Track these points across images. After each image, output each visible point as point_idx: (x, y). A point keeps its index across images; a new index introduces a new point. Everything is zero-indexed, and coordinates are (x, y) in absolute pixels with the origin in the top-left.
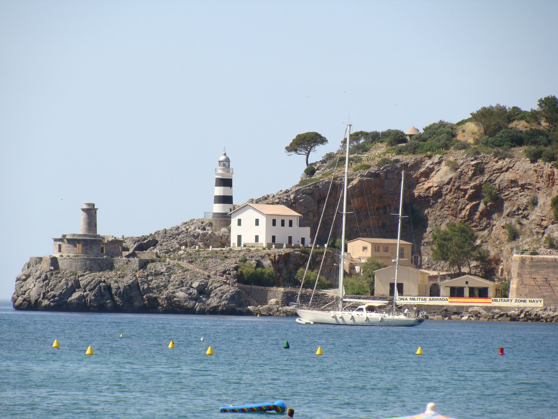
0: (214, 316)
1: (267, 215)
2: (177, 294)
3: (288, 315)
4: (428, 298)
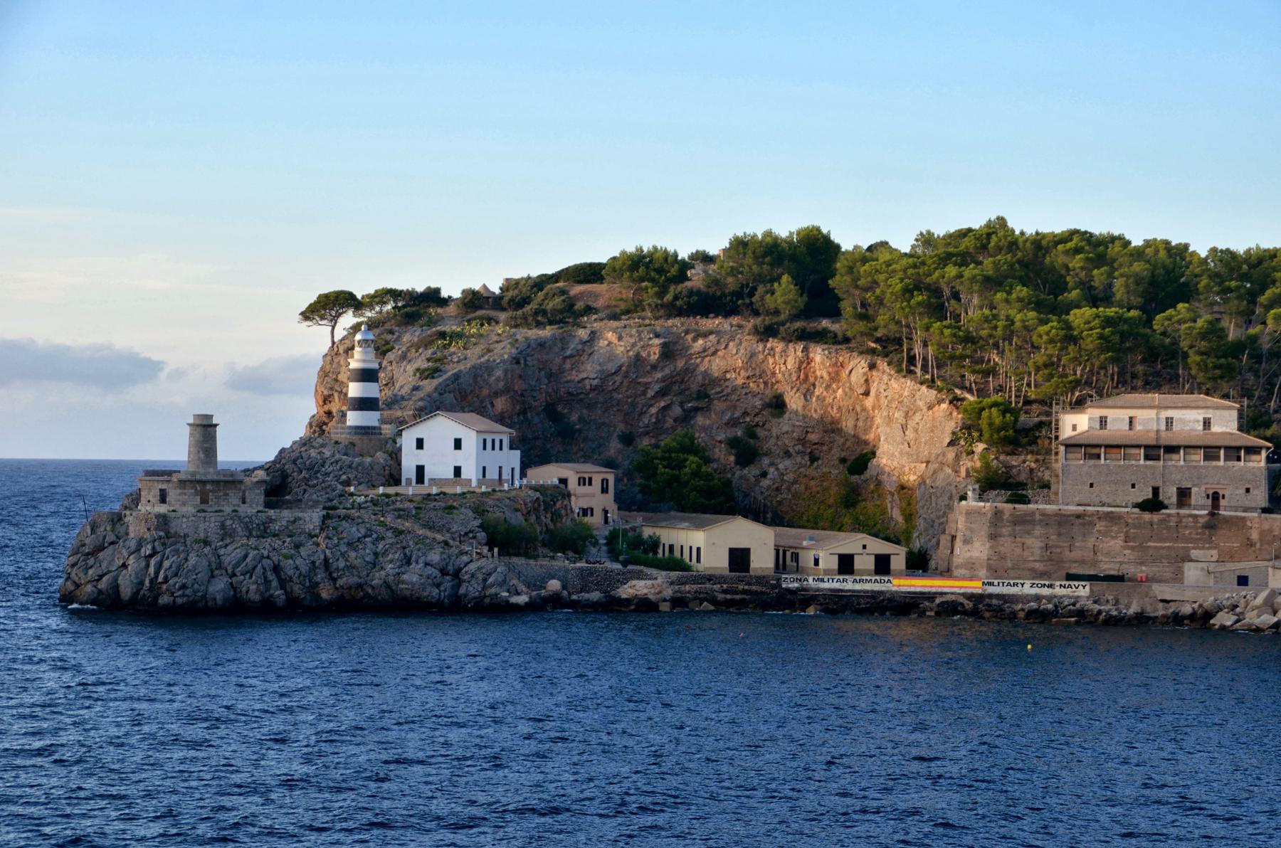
2: (405, 577)
4: (1028, 583)
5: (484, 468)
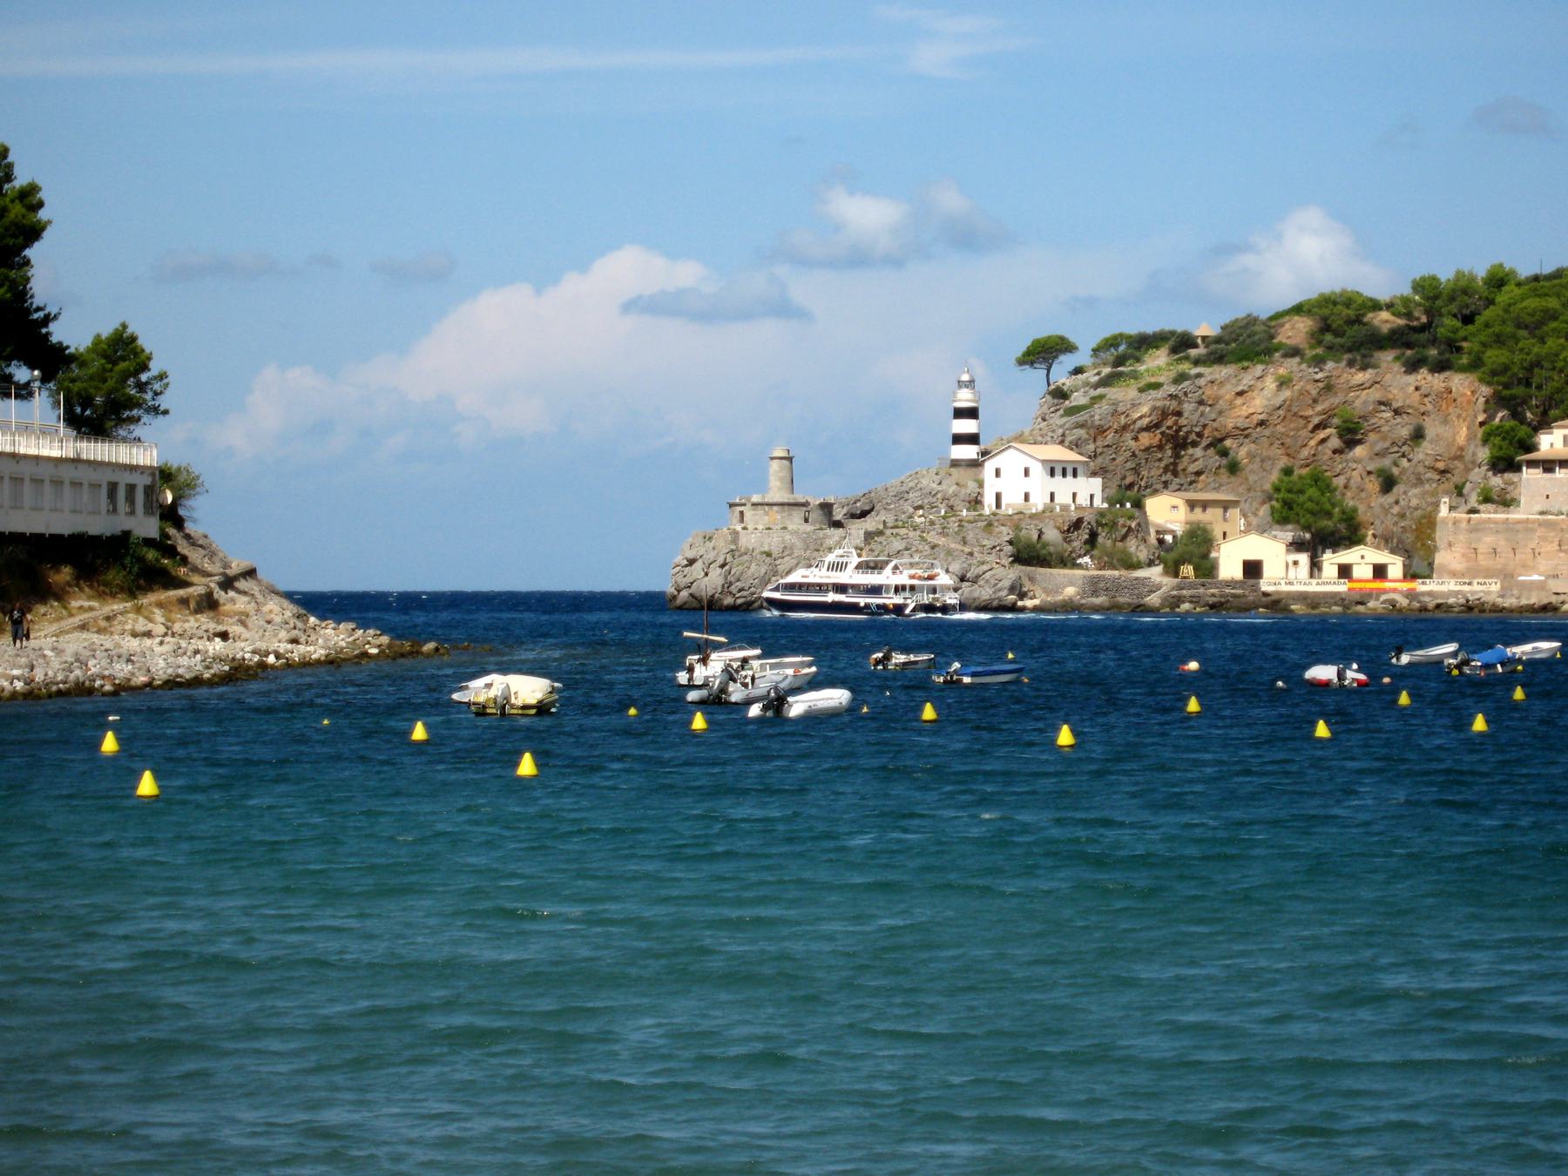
1: (1044, 462)
5: (1052, 495)
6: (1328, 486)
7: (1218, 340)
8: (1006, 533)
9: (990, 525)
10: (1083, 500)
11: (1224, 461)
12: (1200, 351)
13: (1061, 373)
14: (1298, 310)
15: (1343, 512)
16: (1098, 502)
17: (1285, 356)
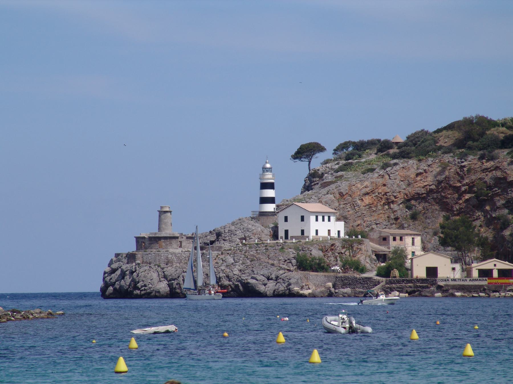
0: (260, 299)
3: (344, 296)
6: (470, 225)
7: (405, 144)
8: (292, 253)
9: (283, 248)
10: (334, 234)
11: (409, 213)
12: (394, 150)
13: (317, 162)
14: (450, 127)
15: (480, 240)
16: (342, 235)
17: (445, 153)
